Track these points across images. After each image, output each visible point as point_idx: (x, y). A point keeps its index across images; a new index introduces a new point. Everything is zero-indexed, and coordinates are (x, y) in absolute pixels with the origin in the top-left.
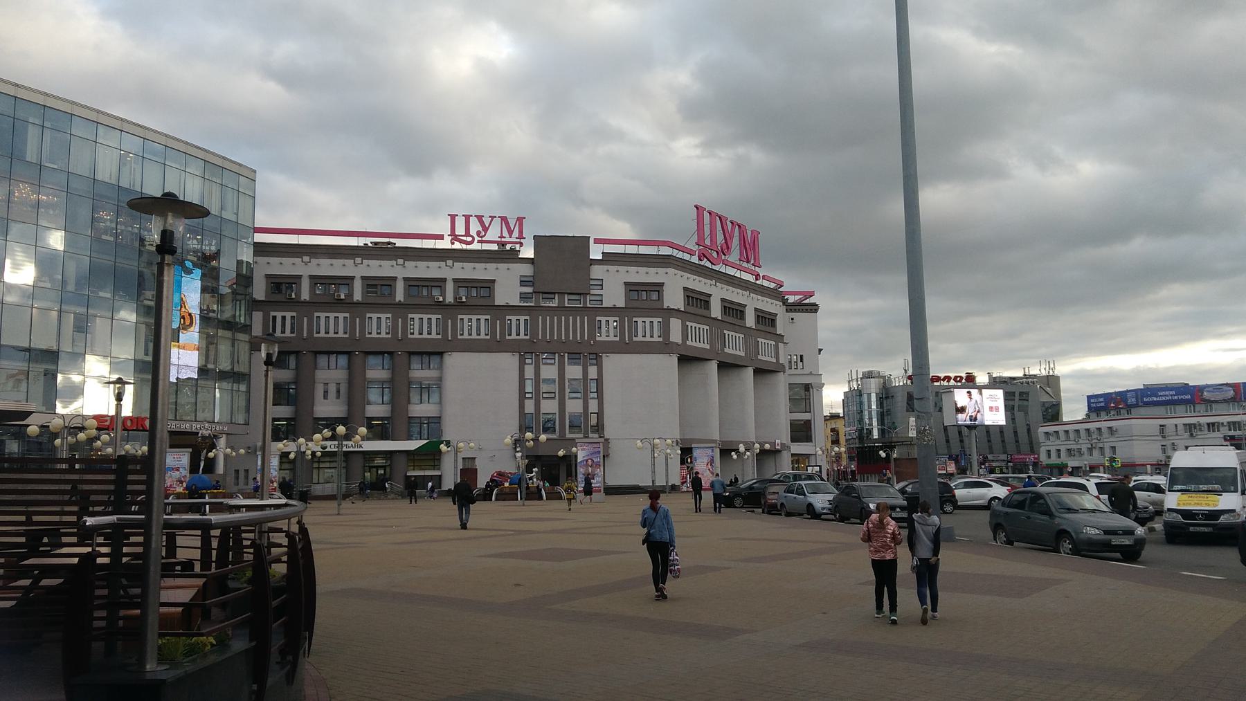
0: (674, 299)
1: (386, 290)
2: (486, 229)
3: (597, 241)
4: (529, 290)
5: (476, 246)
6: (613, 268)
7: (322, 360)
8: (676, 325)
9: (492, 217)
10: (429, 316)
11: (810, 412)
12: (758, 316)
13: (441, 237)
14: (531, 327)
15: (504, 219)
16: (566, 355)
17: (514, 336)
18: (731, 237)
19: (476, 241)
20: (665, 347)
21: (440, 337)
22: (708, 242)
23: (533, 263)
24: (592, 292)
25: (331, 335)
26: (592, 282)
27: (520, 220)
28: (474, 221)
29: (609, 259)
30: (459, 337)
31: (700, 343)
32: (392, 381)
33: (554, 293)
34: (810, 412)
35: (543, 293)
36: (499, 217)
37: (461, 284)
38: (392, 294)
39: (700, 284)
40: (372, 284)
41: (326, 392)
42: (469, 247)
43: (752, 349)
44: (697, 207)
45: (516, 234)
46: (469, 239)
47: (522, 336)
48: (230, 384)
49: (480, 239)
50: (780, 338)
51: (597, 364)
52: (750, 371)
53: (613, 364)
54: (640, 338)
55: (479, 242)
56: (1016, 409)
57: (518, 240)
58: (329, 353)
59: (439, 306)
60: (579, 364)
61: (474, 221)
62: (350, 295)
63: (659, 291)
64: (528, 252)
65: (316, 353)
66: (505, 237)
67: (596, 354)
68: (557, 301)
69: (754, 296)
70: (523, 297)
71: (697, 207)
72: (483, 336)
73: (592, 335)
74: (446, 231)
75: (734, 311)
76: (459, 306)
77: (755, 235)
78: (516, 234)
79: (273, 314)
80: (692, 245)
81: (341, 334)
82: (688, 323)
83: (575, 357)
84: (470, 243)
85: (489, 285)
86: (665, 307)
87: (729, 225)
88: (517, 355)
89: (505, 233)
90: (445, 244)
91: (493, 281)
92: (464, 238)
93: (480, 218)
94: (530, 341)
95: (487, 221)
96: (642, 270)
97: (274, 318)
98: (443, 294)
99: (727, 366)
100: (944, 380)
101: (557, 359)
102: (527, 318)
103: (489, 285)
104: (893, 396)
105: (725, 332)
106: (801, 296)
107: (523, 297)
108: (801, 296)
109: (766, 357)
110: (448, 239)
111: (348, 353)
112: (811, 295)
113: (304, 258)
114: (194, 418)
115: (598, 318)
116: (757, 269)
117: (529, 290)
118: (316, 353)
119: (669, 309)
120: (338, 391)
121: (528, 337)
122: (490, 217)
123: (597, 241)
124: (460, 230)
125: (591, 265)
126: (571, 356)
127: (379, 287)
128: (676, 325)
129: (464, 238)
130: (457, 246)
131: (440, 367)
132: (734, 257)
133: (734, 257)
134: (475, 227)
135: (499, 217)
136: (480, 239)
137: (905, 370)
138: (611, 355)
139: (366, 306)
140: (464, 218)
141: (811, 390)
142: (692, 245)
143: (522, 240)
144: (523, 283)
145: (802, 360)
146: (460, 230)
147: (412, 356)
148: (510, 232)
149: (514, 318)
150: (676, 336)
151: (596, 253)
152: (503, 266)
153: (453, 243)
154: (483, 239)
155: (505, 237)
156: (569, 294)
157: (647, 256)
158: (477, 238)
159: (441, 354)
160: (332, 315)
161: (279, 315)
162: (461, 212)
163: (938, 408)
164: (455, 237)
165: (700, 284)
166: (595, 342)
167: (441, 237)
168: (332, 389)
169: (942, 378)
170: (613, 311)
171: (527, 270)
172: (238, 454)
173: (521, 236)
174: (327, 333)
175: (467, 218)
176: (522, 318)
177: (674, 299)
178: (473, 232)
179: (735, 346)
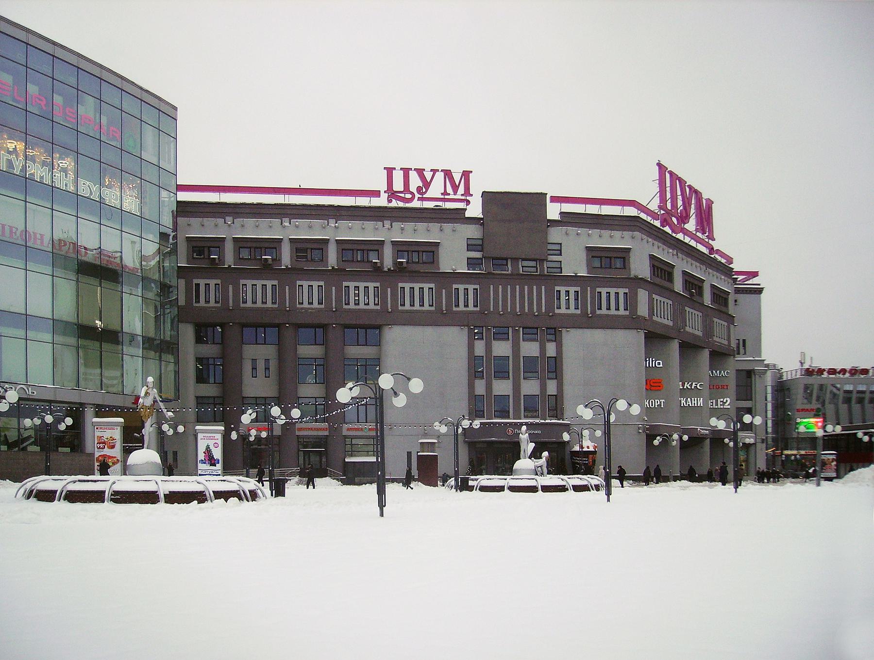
0: (640, 267)
1: (316, 255)
2: (427, 184)
3: (554, 199)
4: (477, 255)
5: (416, 204)
6: (572, 230)
7: (248, 332)
8: (643, 295)
9: (434, 171)
10: (366, 284)
11: (751, 400)
12: (714, 293)
13: (376, 194)
14: (481, 298)
15: (448, 174)
16: (521, 329)
17: (462, 307)
18: (690, 205)
19: (416, 198)
20: (632, 322)
21: (378, 307)
22: (669, 206)
23: (482, 224)
24: (551, 258)
25: (259, 304)
26: (550, 247)
27: (466, 174)
28: (414, 176)
29: (568, 219)
30: (400, 308)
31: (664, 320)
32: (326, 358)
33: (506, 259)
34: (751, 400)
35: (493, 259)
36: (442, 171)
37: (400, 248)
38: (323, 259)
39: (666, 255)
40: (302, 248)
41: (254, 368)
42: (408, 205)
43: (708, 330)
44: (659, 165)
45: (461, 190)
46: (408, 196)
47: (471, 308)
48: (158, 353)
49: (420, 196)
50: (730, 319)
51: (555, 341)
52: (706, 353)
53: (572, 339)
54: (604, 311)
55: (419, 199)
56: (867, 401)
57: (463, 198)
58: (256, 326)
59: (377, 271)
60: (536, 340)
61: (414, 176)
62: (277, 260)
63: (624, 258)
64: (475, 210)
65: (244, 325)
66: (449, 194)
67: (555, 328)
68: (510, 268)
69: (711, 271)
70: (471, 262)
71: (659, 165)
72: (426, 307)
73: (550, 307)
74: (383, 187)
75: (693, 284)
76: (400, 271)
77: (710, 203)
78: (461, 190)
79: (195, 281)
80: (654, 206)
81: (269, 305)
82: (654, 296)
83: (531, 331)
84: (411, 200)
85: (432, 249)
86: (632, 276)
87: (688, 190)
88: (466, 329)
89: (449, 190)
90: (381, 201)
91: (437, 245)
92: (402, 195)
93: (420, 172)
94: (481, 312)
95: (428, 175)
96: (606, 233)
97: (198, 285)
98: (380, 257)
99: (689, 347)
100: (839, 373)
101: (510, 334)
102: (477, 287)
103: (432, 249)
104: (789, 388)
105: (687, 308)
106: (744, 277)
107: (471, 262)
108: (744, 277)
109: (719, 339)
110: (384, 196)
111: (278, 326)
112: (755, 274)
113: (227, 218)
114: (600, 265)
115: (557, 288)
116: (711, 242)
117: (477, 255)
118: (244, 325)
119: (636, 278)
120: (267, 369)
121: (478, 309)
122: (432, 170)
123: (554, 199)
124: (398, 185)
125: (548, 226)
126: (526, 331)
127: (309, 251)
128: (643, 295)
129: (402, 195)
130: (394, 204)
131: (378, 344)
132: (691, 225)
133: (691, 225)
134: (415, 182)
135: (442, 171)
136: (420, 196)
137: (801, 363)
138: (572, 331)
139: (295, 272)
140: (402, 172)
141: (753, 376)
142: (654, 206)
143: (468, 198)
144: (470, 247)
145: (744, 345)
146: (398, 185)
147: (243, 357)
148: (455, 188)
149: (461, 287)
150: (643, 310)
151: (553, 212)
152: (448, 227)
153: (390, 201)
154: (424, 196)
155: (449, 194)
156: (523, 260)
157: (617, 218)
158: (417, 196)
159: (379, 327)
160: (259, 283)
161: (202, 282)
162: (398, 164)
163: (821, 400)
164: (392, 194)
165: (666, 255)
166: (554, 315)
167: (376, 194)
168: (261, 365)
169: (838, 370)
170: (574, 280)
171: (473, 232)
172: (176, 433)
173: (467, 192)
174: (254, 302)
175: (406, 171)
176: (471, 288)
177: (640, 267)
178: (413, 188)
179: (694, 325)
